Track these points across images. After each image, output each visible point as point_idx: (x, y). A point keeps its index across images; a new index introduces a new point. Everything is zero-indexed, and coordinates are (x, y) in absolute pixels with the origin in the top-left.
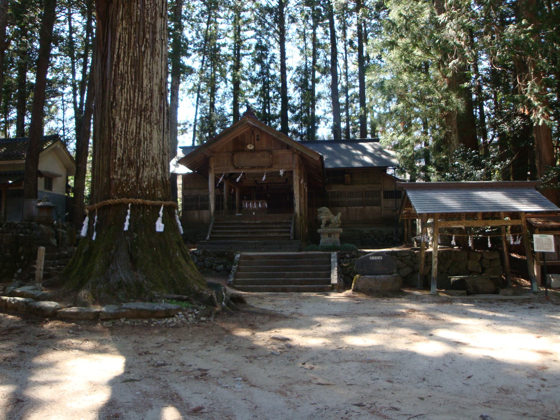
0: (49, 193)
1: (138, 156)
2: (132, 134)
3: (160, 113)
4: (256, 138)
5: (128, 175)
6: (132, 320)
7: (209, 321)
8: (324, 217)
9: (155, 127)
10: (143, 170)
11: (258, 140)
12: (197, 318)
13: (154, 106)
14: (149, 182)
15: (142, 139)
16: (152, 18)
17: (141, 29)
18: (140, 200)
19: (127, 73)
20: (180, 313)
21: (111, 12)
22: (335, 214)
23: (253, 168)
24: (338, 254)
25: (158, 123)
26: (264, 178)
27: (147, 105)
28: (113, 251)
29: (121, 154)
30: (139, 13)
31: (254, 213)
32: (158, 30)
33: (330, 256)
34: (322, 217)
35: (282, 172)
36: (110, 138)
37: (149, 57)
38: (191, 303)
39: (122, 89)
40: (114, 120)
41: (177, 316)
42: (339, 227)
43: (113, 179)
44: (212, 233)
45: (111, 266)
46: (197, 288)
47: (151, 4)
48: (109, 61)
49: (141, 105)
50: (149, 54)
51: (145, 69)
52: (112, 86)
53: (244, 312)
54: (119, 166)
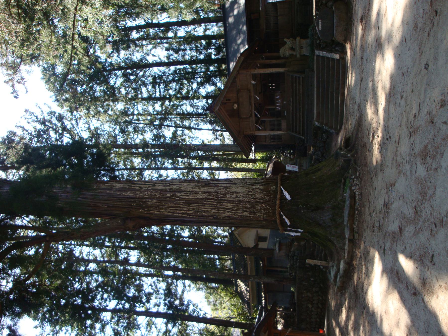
0: (269, 239)
1: (248, 202)
2: (234, 206)
3: (219, 186)
4: (228, 101)
5: (261, 209)
6: (355, 220)
7: (359, 170)
8: (287, 52)
9: (228, 190)
10: (257, 199)
11: (230, 100)
12: (357, 178)
13: (214, 190)
14: (265, 195)
15: (237, 199)
16: (156, 192)
17: (165, 199)
18: (277, 202)
19: (194, 209)
20: (353, 188)
21: (156, 218)
22: (285, 43)
23: (251, 103)
24: (317, 50)
25: (225, 188)
26: (258, 98)
27: (214, 196)
28: (311, 221)
29: (247, 213)
30: (155, 201)
31: (285, 102)
32: (164, 188)
33: (318, 56)
34: (287, 54)
35: (253, 82)
36: (236, 219)
37: (182, 194)
38: (348, 177)
39: (205, 212)
40: (225, 217)
41: (355, 191)
42: (295, 39)
43: (263, 218)
44: (299, 133)
45: (321, 223)
46: (338, 168)
47: (148, 193)
48: (187, 219)
49: (214, 199)
50: (180, 194)
51: (191, 197)
52: (203, 218)
53: (356, 141)
54: (255, 214)
